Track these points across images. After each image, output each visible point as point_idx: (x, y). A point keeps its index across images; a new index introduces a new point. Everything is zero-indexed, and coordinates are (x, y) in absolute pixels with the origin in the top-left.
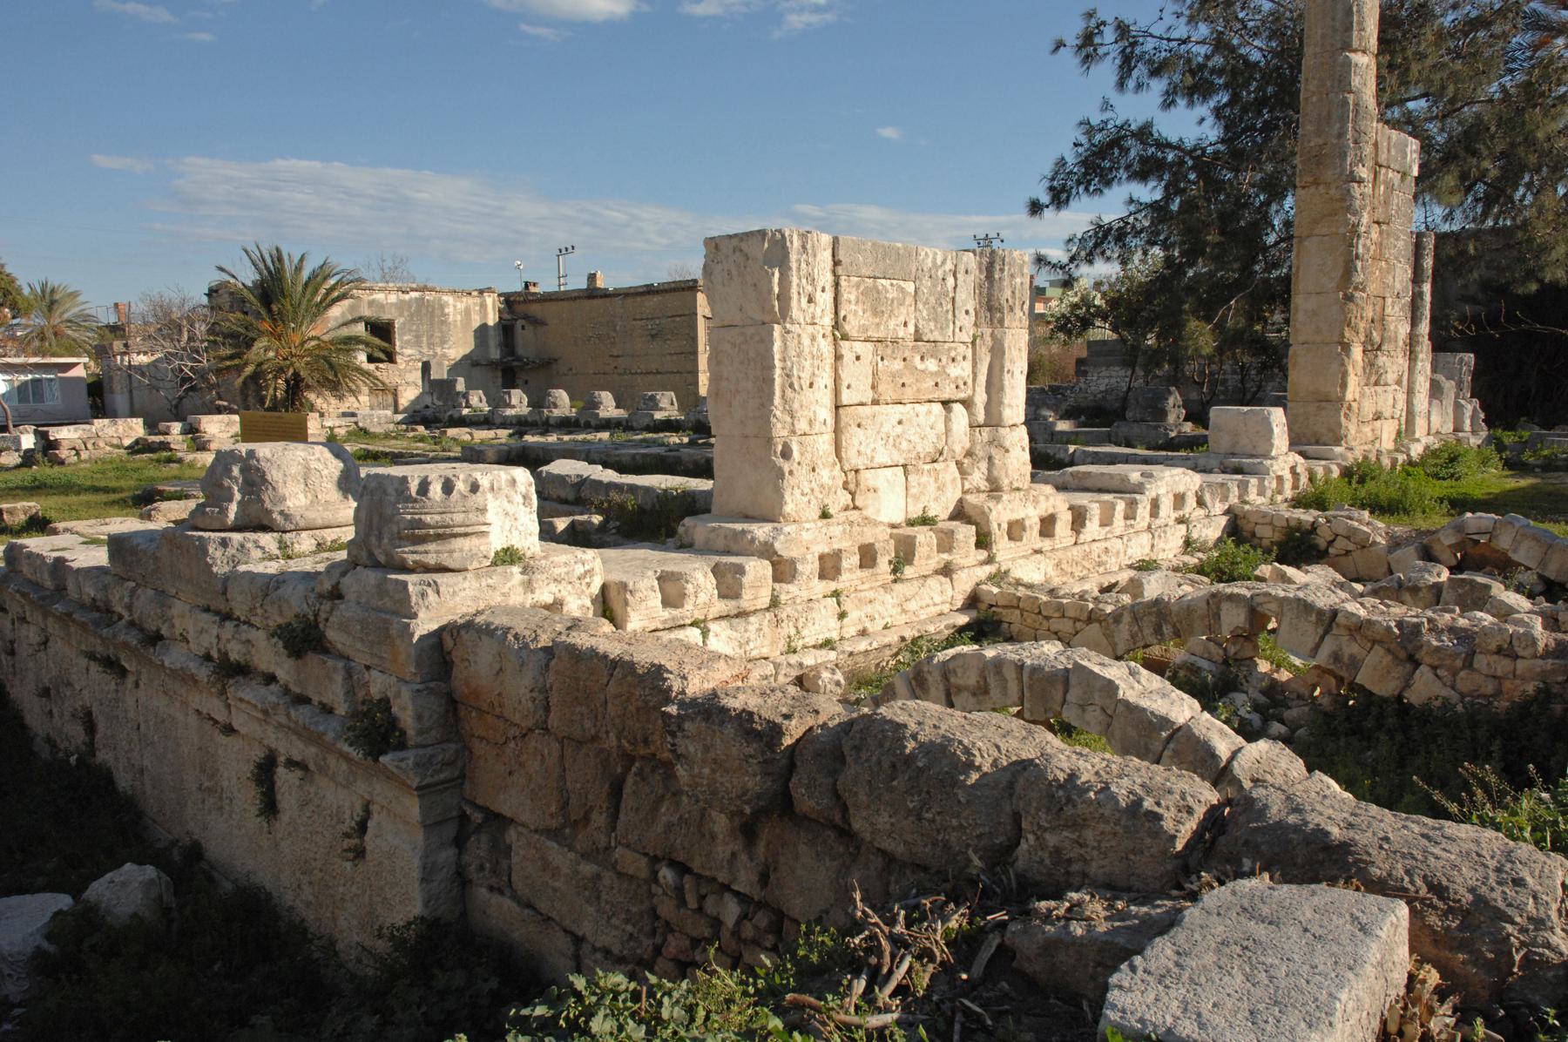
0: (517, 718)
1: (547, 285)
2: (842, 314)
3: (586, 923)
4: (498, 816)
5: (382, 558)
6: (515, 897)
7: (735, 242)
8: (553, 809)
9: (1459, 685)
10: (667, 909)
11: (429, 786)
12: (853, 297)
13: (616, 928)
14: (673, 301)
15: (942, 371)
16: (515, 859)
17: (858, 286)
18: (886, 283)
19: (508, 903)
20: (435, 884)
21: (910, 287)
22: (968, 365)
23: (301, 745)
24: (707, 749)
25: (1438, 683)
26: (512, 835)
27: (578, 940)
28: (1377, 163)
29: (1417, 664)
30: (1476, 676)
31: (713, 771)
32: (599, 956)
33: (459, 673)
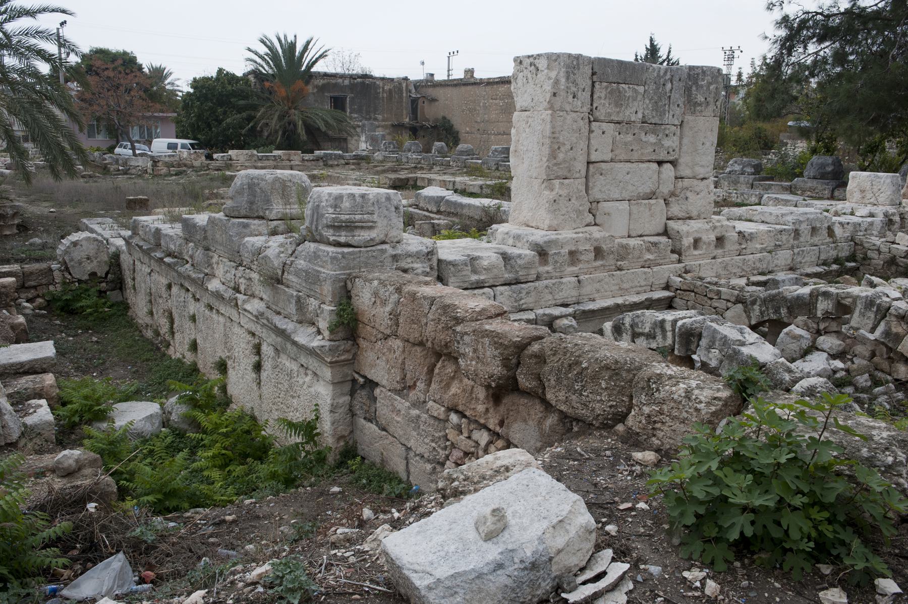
0: (382, 329)
1: (440, 76)
2: (595, 105)
3: (412, 441)
4: (371, 381)
5: (318, 238)
6: (377, 425)
7: (531, 60)
8: (398, 379)
10: (452, 434)
11: (336, 362)
12: (603, 95)
13: (427, 444)
14: (502, 89)
15: (659, 143)
16: (378, 405)
17: (607, 88)
19: (373, 427)
20: (337, 415)
21: (641, 89)
23: (274, 336)
24: (475, 351)
26: (377, 391)
27: (408, 449)
31: (477, 363)
32: (417, 458)
33: (354, 300)
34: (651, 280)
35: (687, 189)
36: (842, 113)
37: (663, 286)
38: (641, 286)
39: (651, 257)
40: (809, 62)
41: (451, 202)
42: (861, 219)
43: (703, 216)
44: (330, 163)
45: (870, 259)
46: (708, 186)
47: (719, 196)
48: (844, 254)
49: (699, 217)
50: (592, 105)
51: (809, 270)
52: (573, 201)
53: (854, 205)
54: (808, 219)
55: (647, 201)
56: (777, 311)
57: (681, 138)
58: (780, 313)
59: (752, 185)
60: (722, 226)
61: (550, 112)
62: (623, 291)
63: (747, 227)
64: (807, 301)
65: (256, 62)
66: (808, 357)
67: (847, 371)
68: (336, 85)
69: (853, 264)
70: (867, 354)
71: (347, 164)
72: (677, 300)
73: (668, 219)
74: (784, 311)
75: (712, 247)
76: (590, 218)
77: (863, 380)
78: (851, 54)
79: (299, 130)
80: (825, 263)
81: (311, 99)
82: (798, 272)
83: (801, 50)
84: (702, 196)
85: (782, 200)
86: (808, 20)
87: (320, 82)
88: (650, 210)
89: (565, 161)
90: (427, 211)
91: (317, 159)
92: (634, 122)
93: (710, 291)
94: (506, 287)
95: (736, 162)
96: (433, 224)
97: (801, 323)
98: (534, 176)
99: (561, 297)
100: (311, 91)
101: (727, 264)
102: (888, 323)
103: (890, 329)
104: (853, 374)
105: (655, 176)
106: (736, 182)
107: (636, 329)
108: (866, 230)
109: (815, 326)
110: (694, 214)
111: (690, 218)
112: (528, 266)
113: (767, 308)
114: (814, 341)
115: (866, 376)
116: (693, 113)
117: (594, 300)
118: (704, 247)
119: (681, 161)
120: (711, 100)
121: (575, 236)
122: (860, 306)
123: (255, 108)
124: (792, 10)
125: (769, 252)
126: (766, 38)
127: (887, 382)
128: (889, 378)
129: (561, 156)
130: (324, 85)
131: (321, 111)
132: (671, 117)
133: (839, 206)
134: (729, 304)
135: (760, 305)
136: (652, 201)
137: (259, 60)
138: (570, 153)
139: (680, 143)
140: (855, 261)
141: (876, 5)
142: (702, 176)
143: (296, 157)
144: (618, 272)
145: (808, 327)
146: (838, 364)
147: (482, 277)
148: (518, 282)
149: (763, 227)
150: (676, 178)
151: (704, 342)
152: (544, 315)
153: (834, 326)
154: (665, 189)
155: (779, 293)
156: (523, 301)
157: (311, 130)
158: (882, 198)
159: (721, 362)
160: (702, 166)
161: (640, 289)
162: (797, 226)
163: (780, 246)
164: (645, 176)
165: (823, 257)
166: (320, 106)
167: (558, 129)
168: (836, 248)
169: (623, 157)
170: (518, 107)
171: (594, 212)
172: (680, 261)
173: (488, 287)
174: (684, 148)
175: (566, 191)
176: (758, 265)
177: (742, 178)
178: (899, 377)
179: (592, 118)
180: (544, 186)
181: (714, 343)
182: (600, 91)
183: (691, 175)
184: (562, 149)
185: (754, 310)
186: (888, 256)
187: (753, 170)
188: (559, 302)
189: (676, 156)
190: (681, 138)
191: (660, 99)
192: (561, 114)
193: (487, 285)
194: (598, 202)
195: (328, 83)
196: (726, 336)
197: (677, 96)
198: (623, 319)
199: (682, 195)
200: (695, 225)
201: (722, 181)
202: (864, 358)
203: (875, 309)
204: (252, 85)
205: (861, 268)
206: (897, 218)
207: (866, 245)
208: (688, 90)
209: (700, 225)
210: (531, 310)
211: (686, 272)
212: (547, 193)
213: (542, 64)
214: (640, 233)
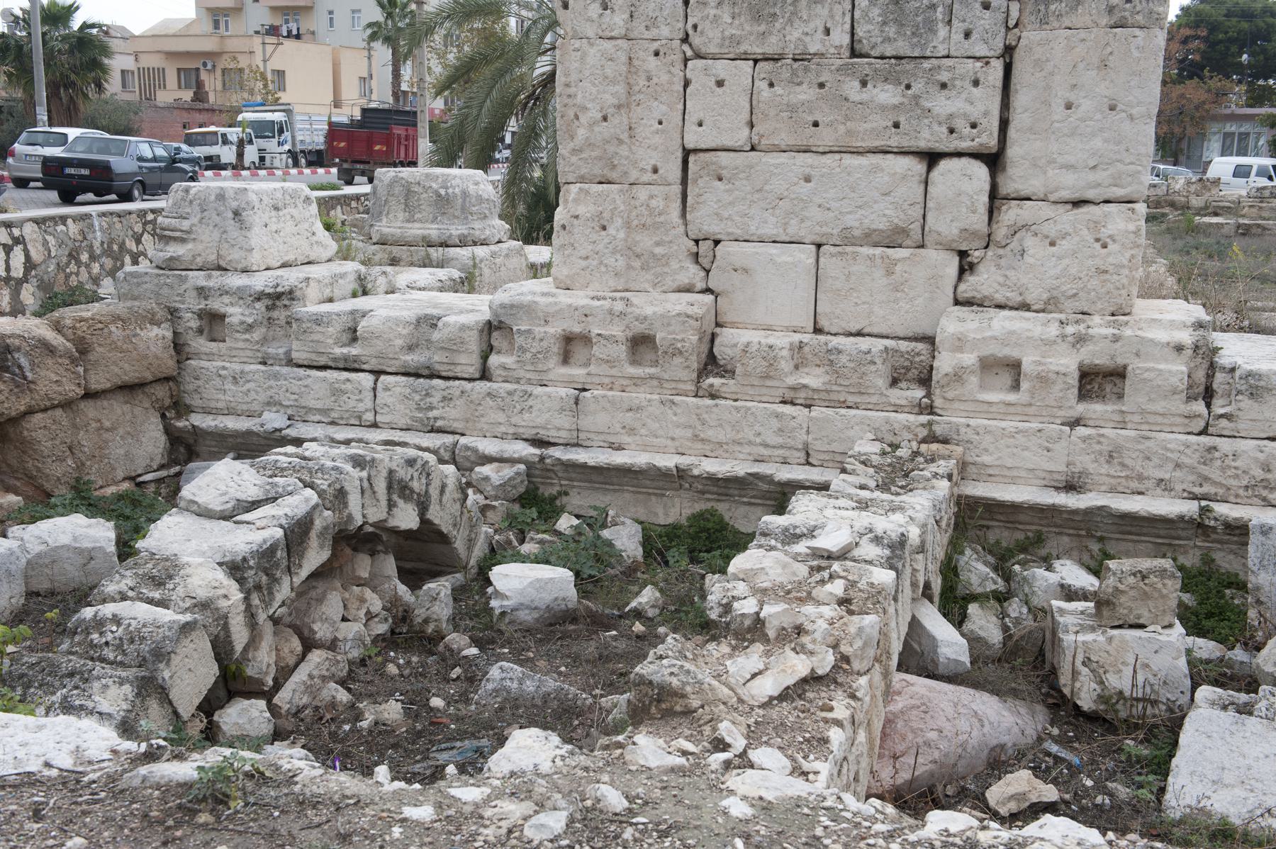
34: (802, 437)
38: (766, 446)
76: (692, 274)
88: (889, 273)
94: (404, 378)
132: (958, 37)
156: (435, 413)
160: (1069, 167)
169: (784, 139)
175: (592, 208)
184: (583, 119)
192: (577, 44)
193: (365, 367)
194: (717, 242)
199: (1014, 244)
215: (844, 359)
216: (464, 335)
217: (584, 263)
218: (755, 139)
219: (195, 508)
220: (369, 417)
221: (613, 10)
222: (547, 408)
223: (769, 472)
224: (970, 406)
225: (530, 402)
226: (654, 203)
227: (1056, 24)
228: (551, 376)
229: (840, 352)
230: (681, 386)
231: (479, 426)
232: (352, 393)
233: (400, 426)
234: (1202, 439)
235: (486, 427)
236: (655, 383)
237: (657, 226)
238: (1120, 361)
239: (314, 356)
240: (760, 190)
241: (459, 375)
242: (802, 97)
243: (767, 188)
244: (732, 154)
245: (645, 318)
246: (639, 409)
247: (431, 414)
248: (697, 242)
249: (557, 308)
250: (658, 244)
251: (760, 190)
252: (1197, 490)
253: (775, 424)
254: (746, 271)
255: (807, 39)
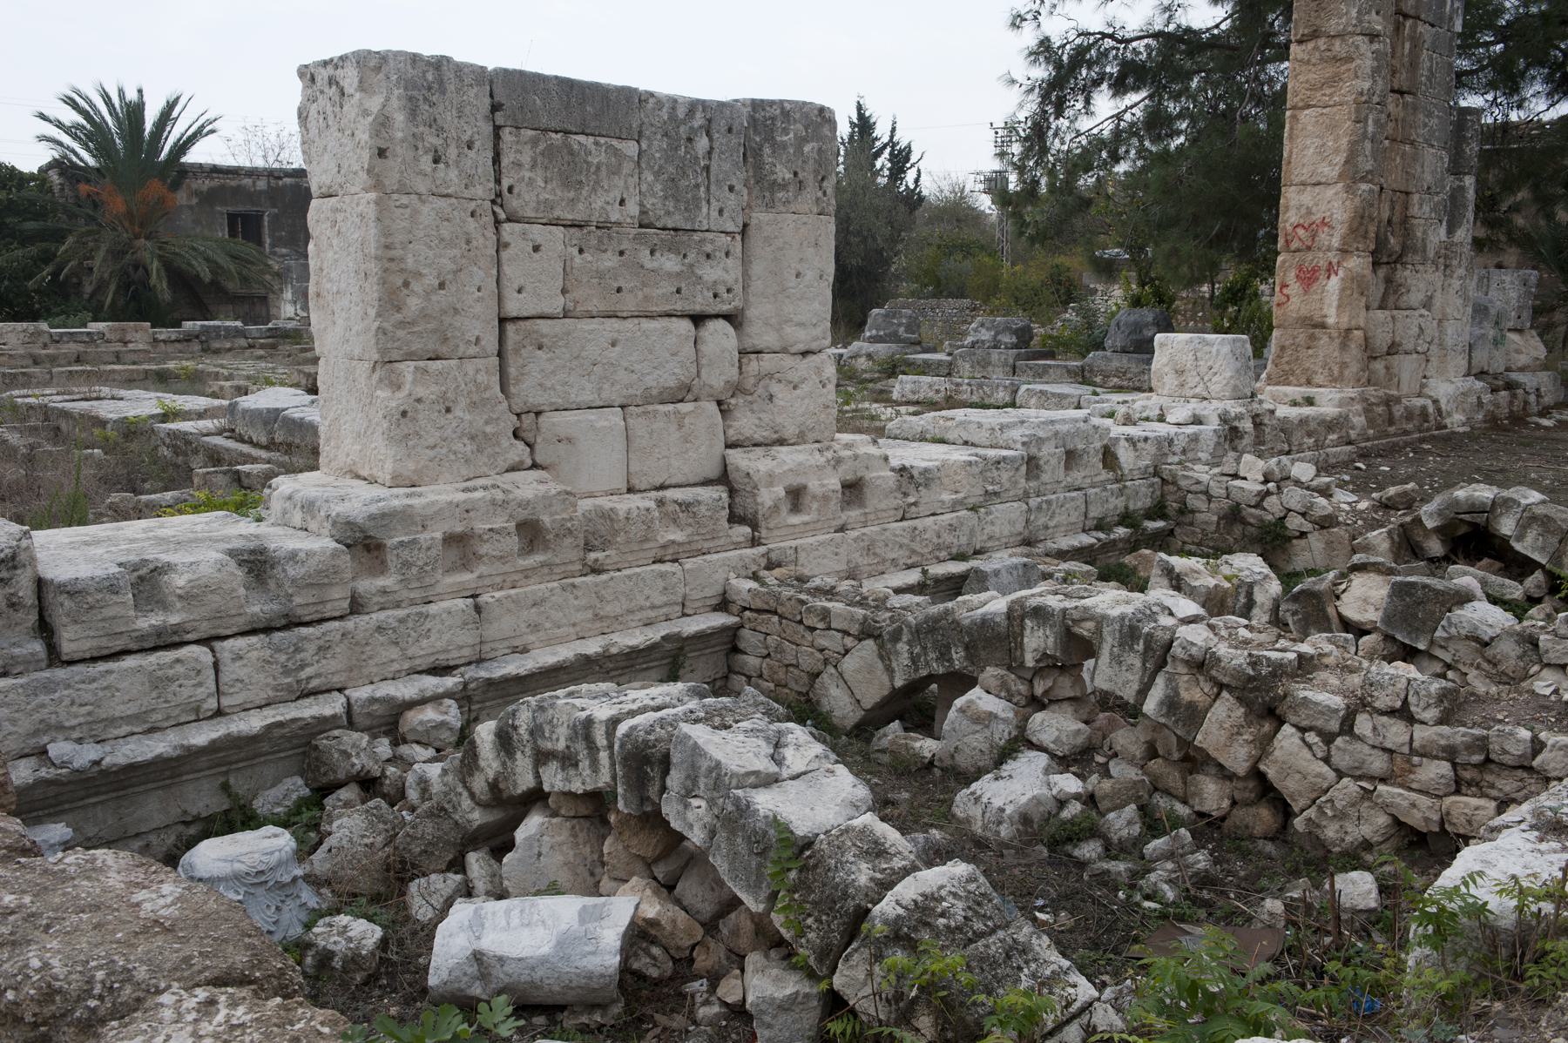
2: (505, 183)
7: (330, 70)
9: (1335, 759)
12: (526, 158)
17: (534, 142)
18: (589, 141)
21: (631, 148)
22: (733, 264)
25: (1306, 754)
28: (1399, 12)
29: (1281, 722)
30: (1358, 746)
34: (681, 590)
35: (770, 376)
36: (1164, 225)
37: (714, 602)
38: (653, 607)
39: (677, 535)
40: (1106, 133)
41: (293, 420)
42: (1173, 430)
43: (811, 436)
44: (216, 345)
45: (1193, 512)
46: (819, 371)
47: (938, 391)
48: (1141, 503)
49: (801, 438)
50: (498, 181)
51: (1065, 543)
52: (458, 412)
53: (1165, 401)
54: (1056, 433)
55: (671, 407)
56: (944, 655)
57: (746, 261)
58: (950, 660)
59: (1014, 368)
60: (856, 457)
61: (372, 195)
62: (604, 623)
63: (920, 456)
64: (1003, 630)
65: (60, 143)
66: (1009, 767)
67: (1090, 800)
68: (238, 190)
69: (1160, 524)
70: (1138, 751)
71: (251, 346)
72: (745, 633)
73: (728, 446)
74: (958, 656)
75: (834, 505)
76: (519, 451)
77: (1122, 822)
78: (1180, 116)
79: (154, 280)
80: (1100, 526)
81: (186, 218)
82: (1040, 548)
83: (1079, 105)
84: (807, 391)
85: (1053, 395)
86: (1090, 47)
87: (205, 184)
88: (680, 426)
89: (425, 315)
90: (251, 442)
91: (188, 338)
92: (619, 224)
93: (809, 610)
94: (253, 639)
95: (982, 325)
96: (238, 472)
97: (993, 683)
98: (357, 352)
99: (425, 650)
100: (184, 202)
101: (873, 543)
102: (1170, 680)
103: (1177, 694)
104: (1103, 805)
105: (689, 349)
106: (985, 364)
107: (540, 742)
108: (1184, 452)
109: (1023, 688)
110: (790, 432)
111: (782, 442)
112: (321, 579)
113: (924, 648)
114: (1022, 728)
115: (1130, 810)
116: (770, 206)
117: (525, 650)
118: (815, 505)
119: (752, 313)
120: (807, 175)
121: (461, 496)
122: (1109, 639)
123: (59, 236)
124: (1057, 29)
125: (974, 509)
126: (1013, 81)
127: (1177, 823)
128: (1182, 810)
129: (414, 304)
130: (212, 191)
131: (204, 243)
132: (714, 214)
133: (1139, 402)
134: (849, 641)
135: (909, 643)
136: (685, 407)
137: (66, 140)
138: (440, 298)
139: (746, 274)
140: (1163, 517)
141: (1217, 26)
142: (801, 347)
143: (138, 336)
144: (590, 579)
145: (1008, 691)
146: (1069, 784)
147: (174, 619)
148: (292, 623)
149: (959, 455)
150: (743, 352)
151: (675, 779)
152: (373, 700)
153: (1065, 687)
154: (718, 376)
155: (947, 612)
156: (309, 671)
157: (181, 280)
158: (1217, 385)
159: (712, 833)
160: (801, 325)
161: (652, 614)
162: (1033, 451)
163: (995, 493)
164: (662, 350)
165: (1095, 512)
166: (207, 233)
167: (398, 238)
168: (1121, 492)
169: (596, 305)
170: (314, 189)
171: (529, 436)
172: (754, 542)
173: (197, 642)
174: (757, 285)
176: (948, 538)
177: (995, 355)
178: (1205, 808)
179: (501, 210)
180: (376, 376)
181: (695, 780)
182: (517, 148)
183: (777, 346)
184: (415, 286)
185: (897, 653)
186: (1226, 504)
187: (1014, 340)
188: (424, 663)
189: (737, 303)
190: (746, 261)
191: (682, 171)
192: (405, 200)
193: (190, 637)
194: (538, 414)
195: (222, 187)
196: (718, 764)
197: (727, 166)
198: (514, 714)
199: (760, 391)
200: (788, 457)
201: (960, 362)
202: (1131, 761)
203: (1140, 647)
204: (56, 189)
205: (1178, 531)
206: (1247, 425)
207: (1183, 483)
208: (751, 155)
209: (801, 457)
210: (340, 690)
211: (770, 566)
212: (382, 394)
213: (350, 78)
214: (658, 481)
215: (703, 509)
216: (338, 562)
217: (431, 453)
218: (570, 305)
219: (752, 779)
220: (212, 704)
221: (447, 165)
222: (445, 625)
223: (676, 630)
224: (783, 532)
225: (428, 625)
226: (480, 378)
227: (782, 209)
228: (439, 589)
229: (699, 503)
230: (570, 568)
231: (365, 671)
232: (187, 677)
233: (258, 703)
234: (905, 524)
235: (375, 670)
236: (546, 570)
237: (484, 402)
238: (859, 474)
239: (104, 642)
240: (577, 358)
241: (327, 615)
242: (609, 264)
243: (584, 354)
244: (549, 322)
245: (528, 502)
246: (543, 600)
247: (303, 675)
248: (518, 415)
249: (436, 508)
250: (487, 423)
251: (577, 358)
252: (909, 562)
253: (661, 584)
254: (569, 440)
255: (609, 208)
